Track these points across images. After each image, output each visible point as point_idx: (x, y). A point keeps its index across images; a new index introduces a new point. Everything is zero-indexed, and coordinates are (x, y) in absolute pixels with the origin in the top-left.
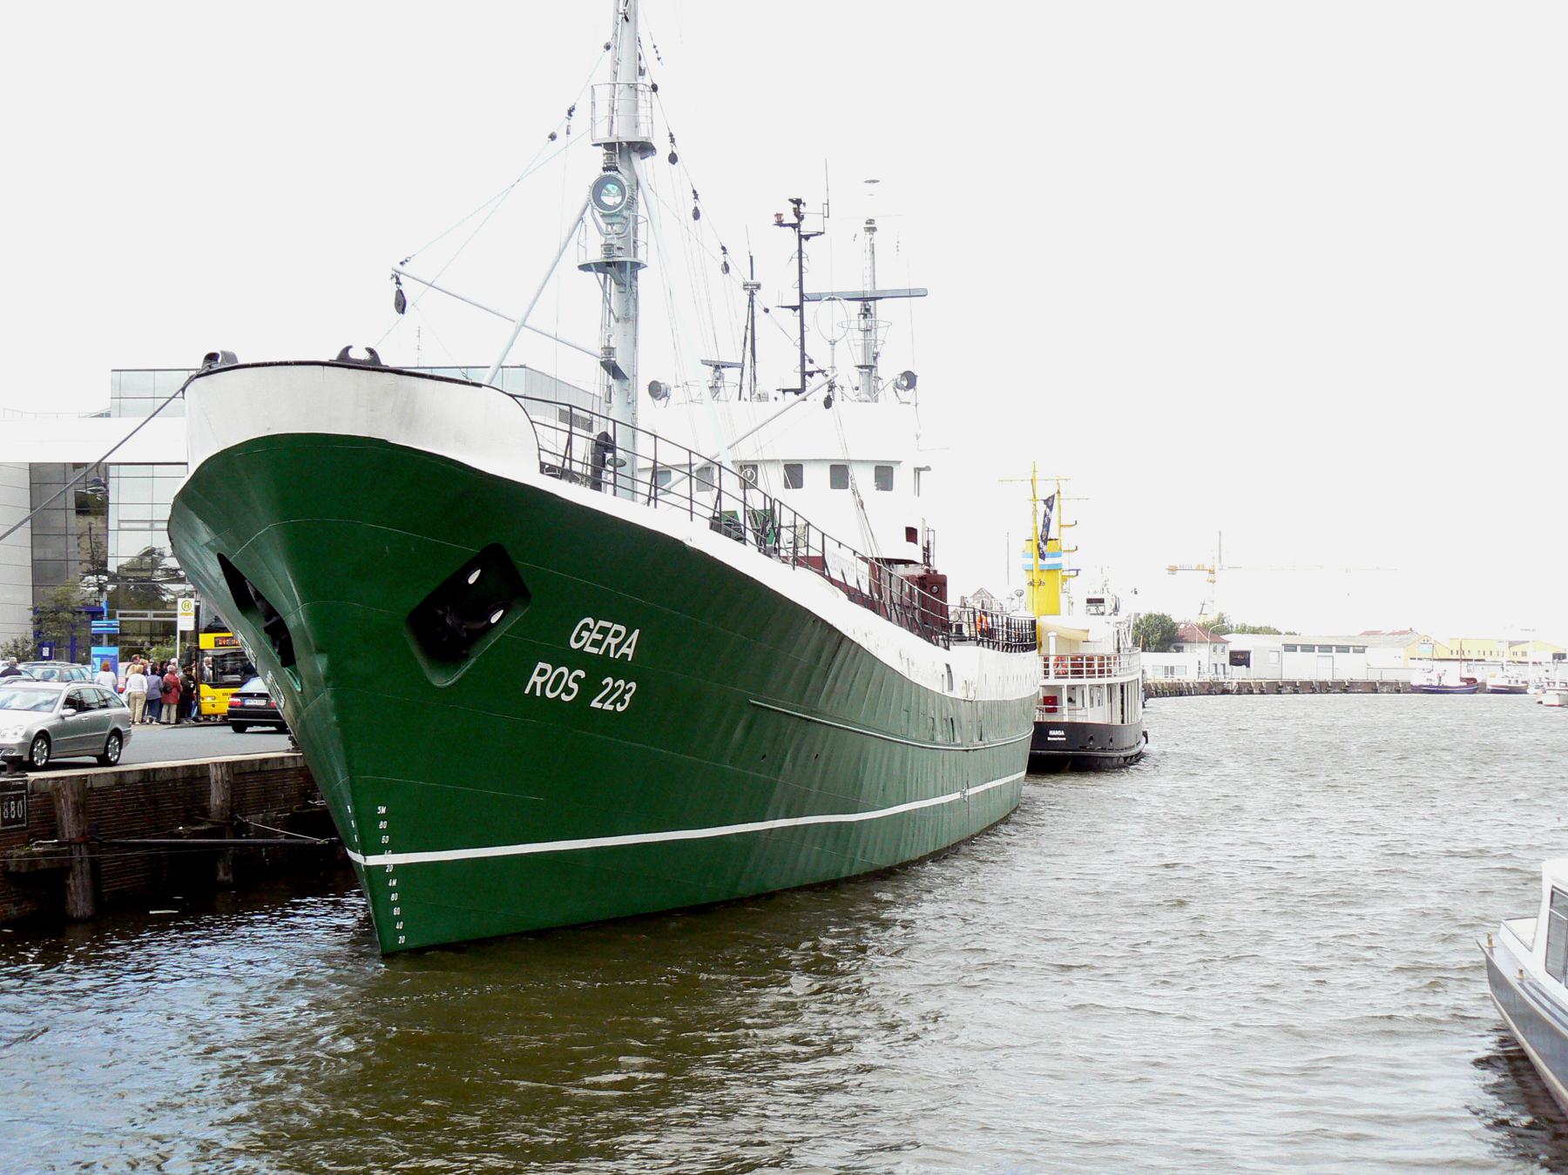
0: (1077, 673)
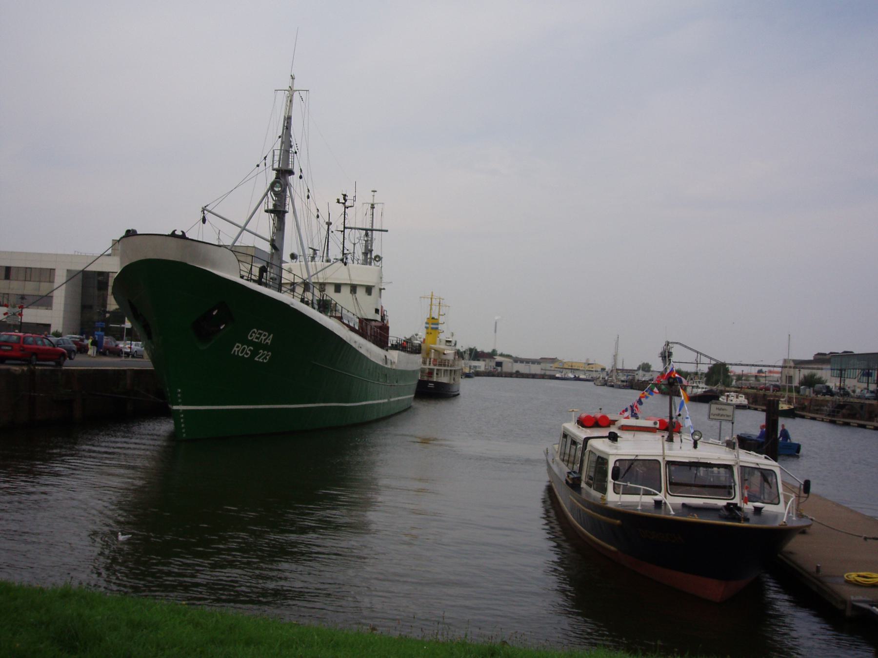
0: (440, 365)
